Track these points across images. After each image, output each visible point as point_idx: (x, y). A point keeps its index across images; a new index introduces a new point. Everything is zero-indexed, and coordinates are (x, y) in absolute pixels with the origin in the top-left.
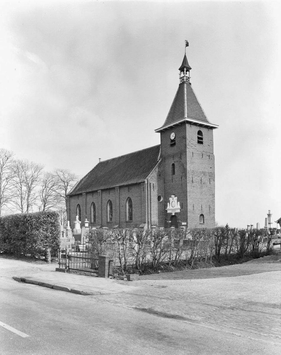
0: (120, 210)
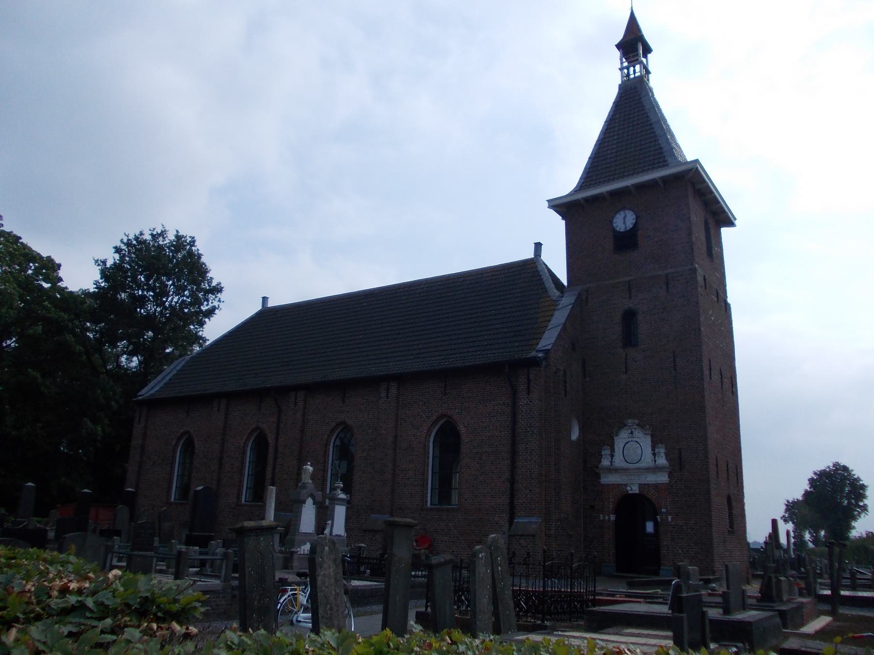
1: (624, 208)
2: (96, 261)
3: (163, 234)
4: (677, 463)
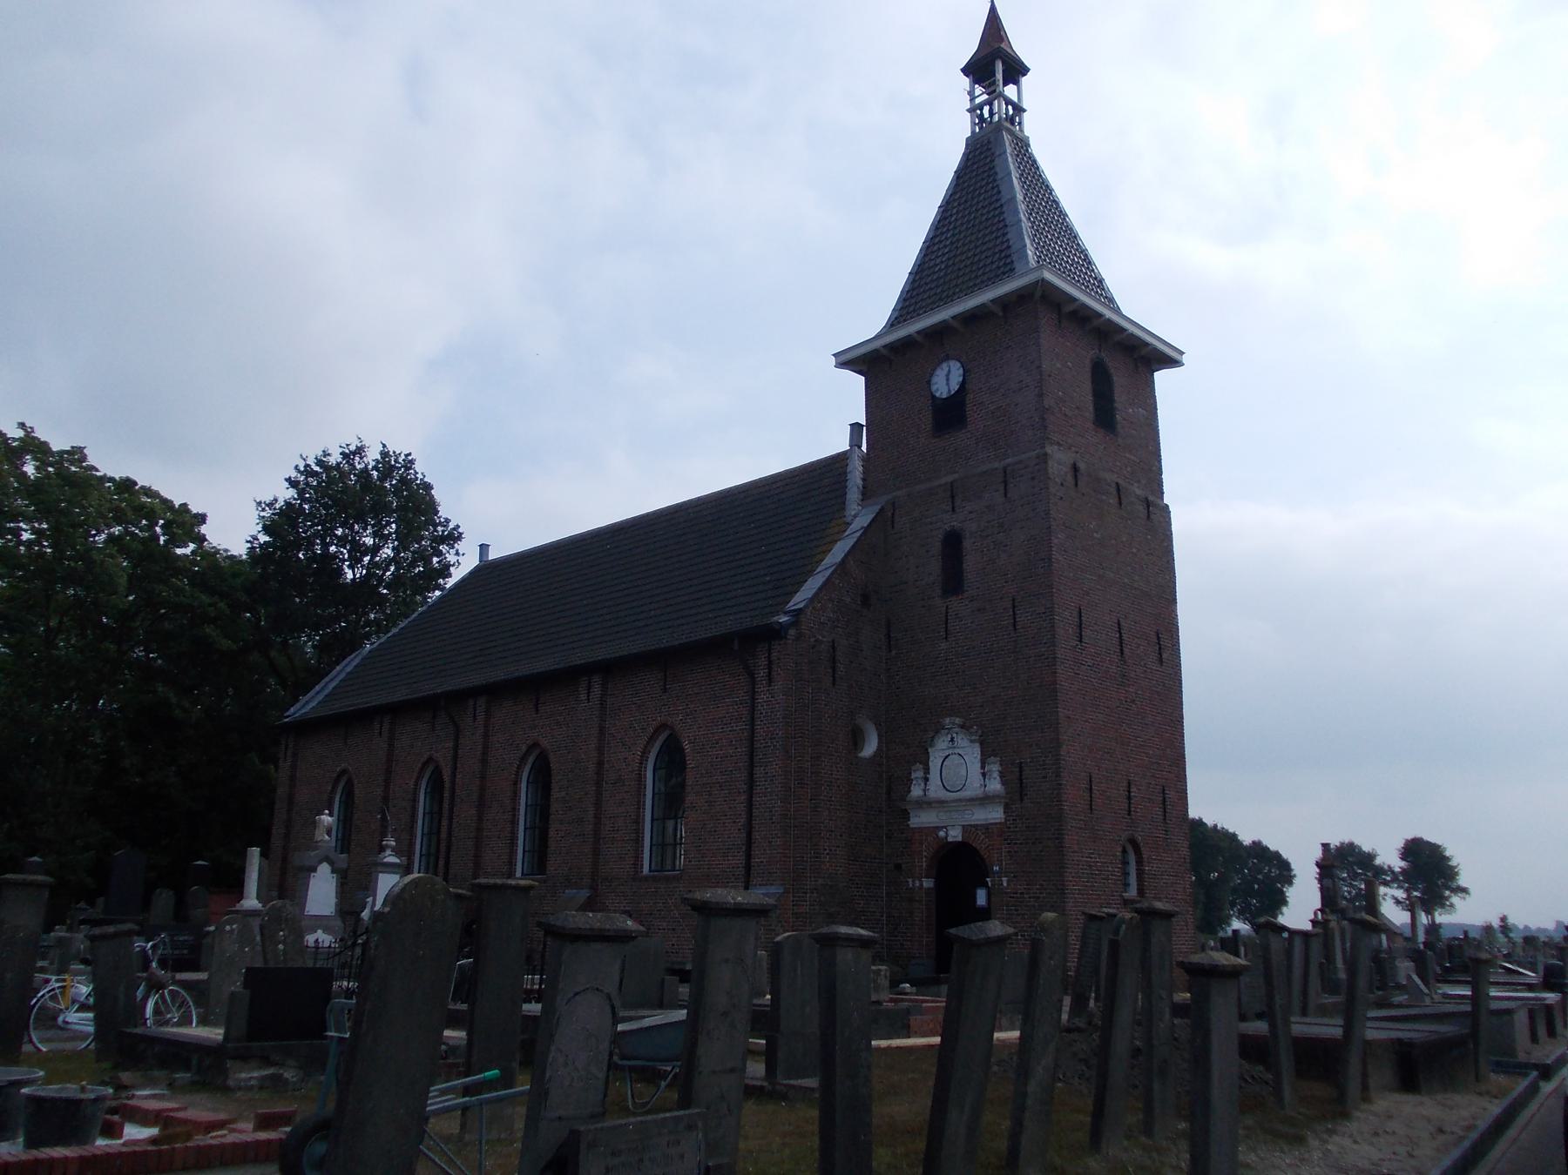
0: (598, 804)
1: (947, 358)
2: (259, 504)
3: (360, 451)
4: (1017, 789)
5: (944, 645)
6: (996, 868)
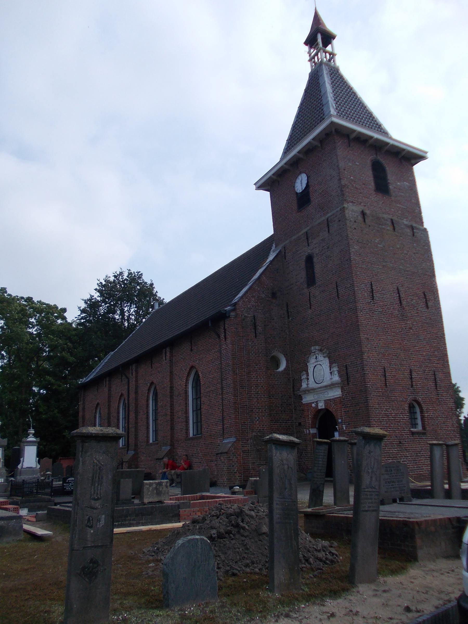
1: (301, 173)
3: (121, 273)
5: (310, 311)
6: (340, 421)
